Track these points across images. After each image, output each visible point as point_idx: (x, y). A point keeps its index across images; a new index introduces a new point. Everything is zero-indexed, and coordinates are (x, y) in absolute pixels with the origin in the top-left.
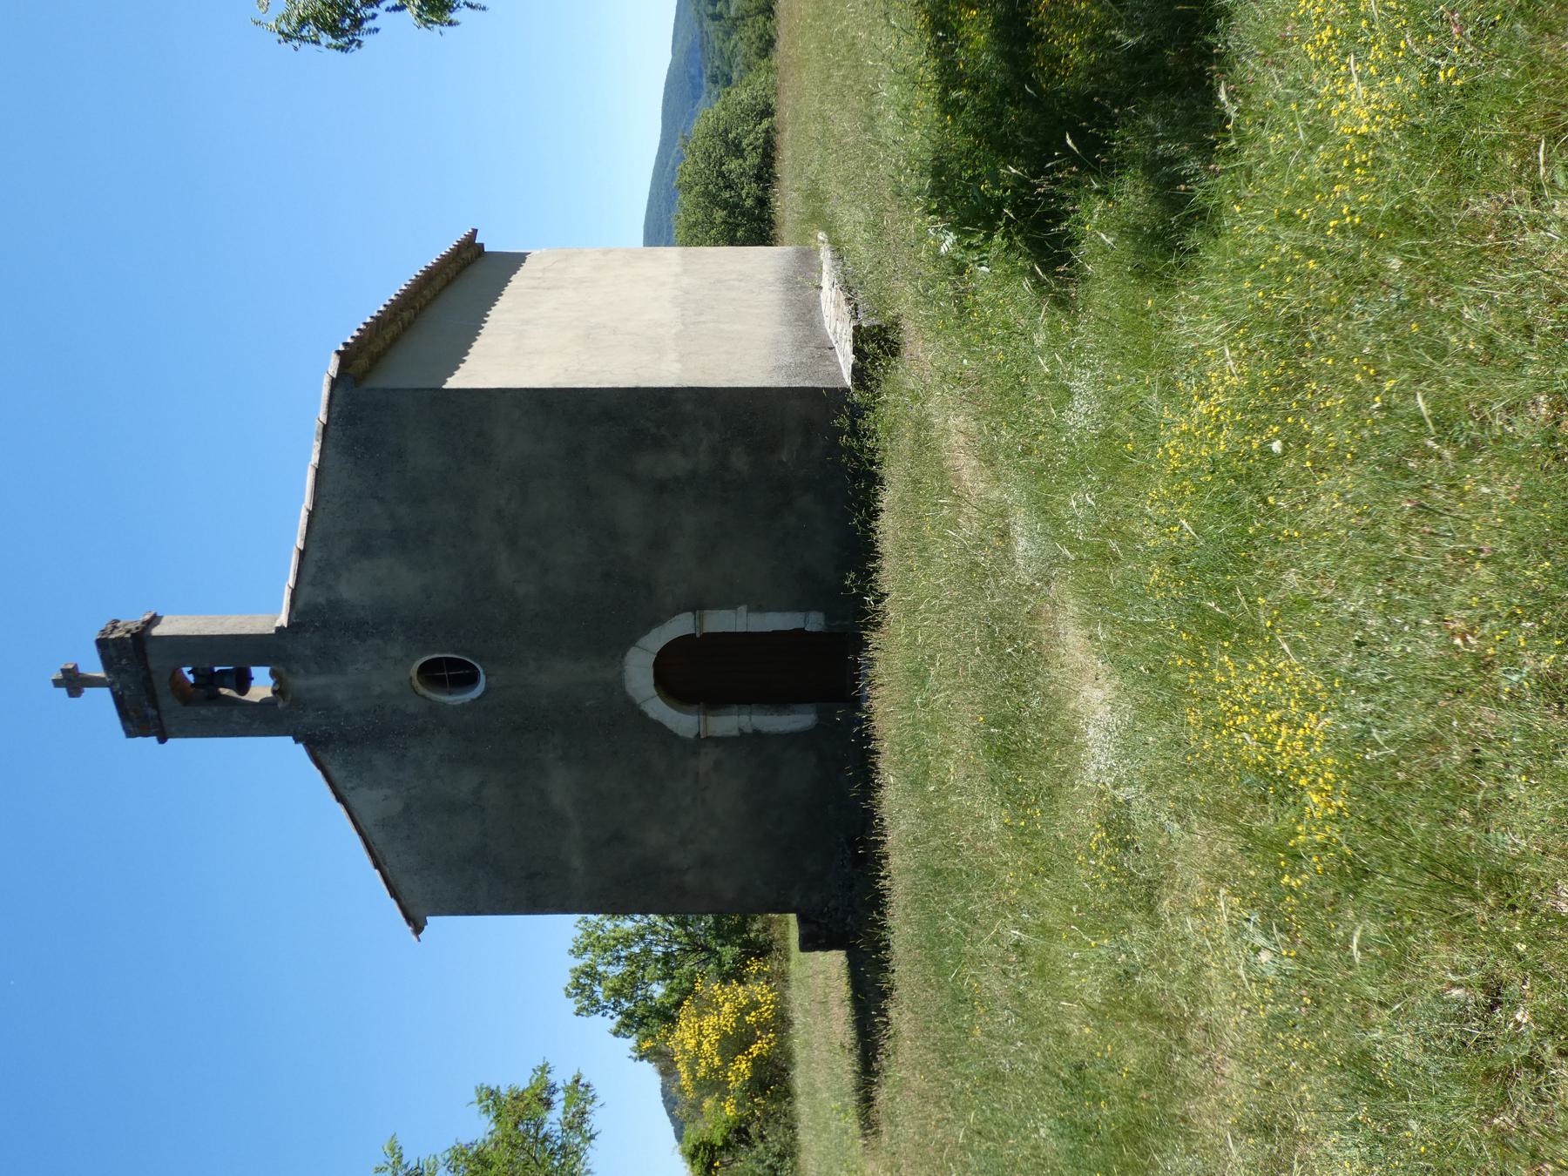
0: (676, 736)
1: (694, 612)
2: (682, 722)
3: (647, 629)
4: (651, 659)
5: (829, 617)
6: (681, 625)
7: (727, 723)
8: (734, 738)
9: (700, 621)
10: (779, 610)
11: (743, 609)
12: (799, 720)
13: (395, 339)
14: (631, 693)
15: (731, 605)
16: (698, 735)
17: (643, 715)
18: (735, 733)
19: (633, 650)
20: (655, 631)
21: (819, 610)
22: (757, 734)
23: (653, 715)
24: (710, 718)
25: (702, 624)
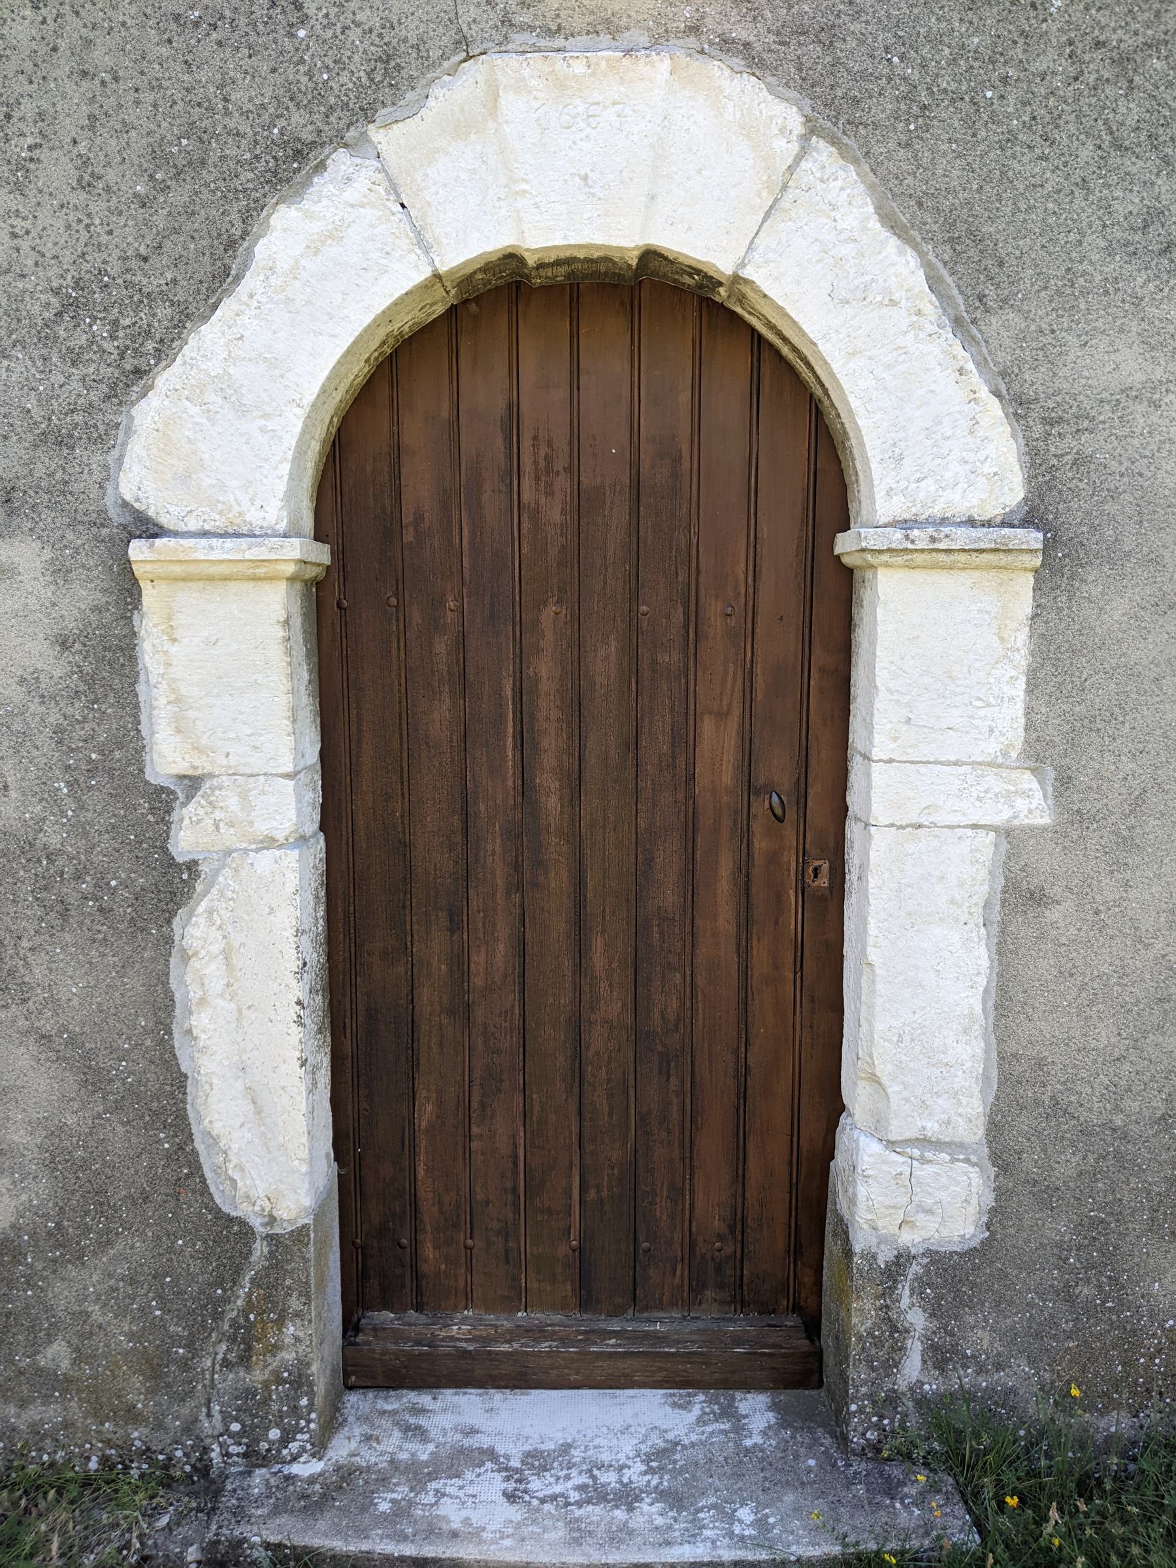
0: (135, 377)
1: (1030, 517)
2: (231, 434)
3: (912, 210)
4: (703, 240)
5: (951, 1278)
6: (924, 427)
7: (233, 711)
8: (130, 742)
9: (935, 543)
10: (1005, 1001)
11: (1030, 803)
12: (266, 1128)
13: (226, 579)
14: (454, 93)
15: (1056, 744)
16: (148, 528)
17: (291, 165)
18: (167, 758)
19: (783, 116)
20: (901, 268)
21: (997, 1216)
22: (172, 885)
23: (286, 234)
24: (823, 151)
25: (942, 557)
